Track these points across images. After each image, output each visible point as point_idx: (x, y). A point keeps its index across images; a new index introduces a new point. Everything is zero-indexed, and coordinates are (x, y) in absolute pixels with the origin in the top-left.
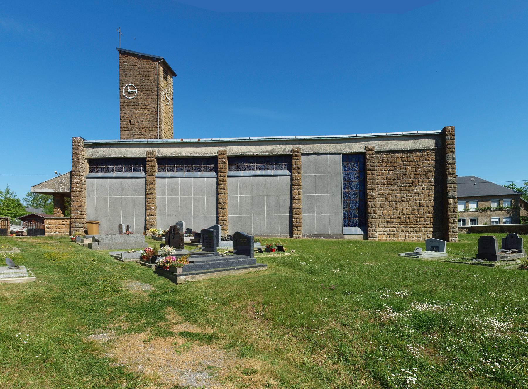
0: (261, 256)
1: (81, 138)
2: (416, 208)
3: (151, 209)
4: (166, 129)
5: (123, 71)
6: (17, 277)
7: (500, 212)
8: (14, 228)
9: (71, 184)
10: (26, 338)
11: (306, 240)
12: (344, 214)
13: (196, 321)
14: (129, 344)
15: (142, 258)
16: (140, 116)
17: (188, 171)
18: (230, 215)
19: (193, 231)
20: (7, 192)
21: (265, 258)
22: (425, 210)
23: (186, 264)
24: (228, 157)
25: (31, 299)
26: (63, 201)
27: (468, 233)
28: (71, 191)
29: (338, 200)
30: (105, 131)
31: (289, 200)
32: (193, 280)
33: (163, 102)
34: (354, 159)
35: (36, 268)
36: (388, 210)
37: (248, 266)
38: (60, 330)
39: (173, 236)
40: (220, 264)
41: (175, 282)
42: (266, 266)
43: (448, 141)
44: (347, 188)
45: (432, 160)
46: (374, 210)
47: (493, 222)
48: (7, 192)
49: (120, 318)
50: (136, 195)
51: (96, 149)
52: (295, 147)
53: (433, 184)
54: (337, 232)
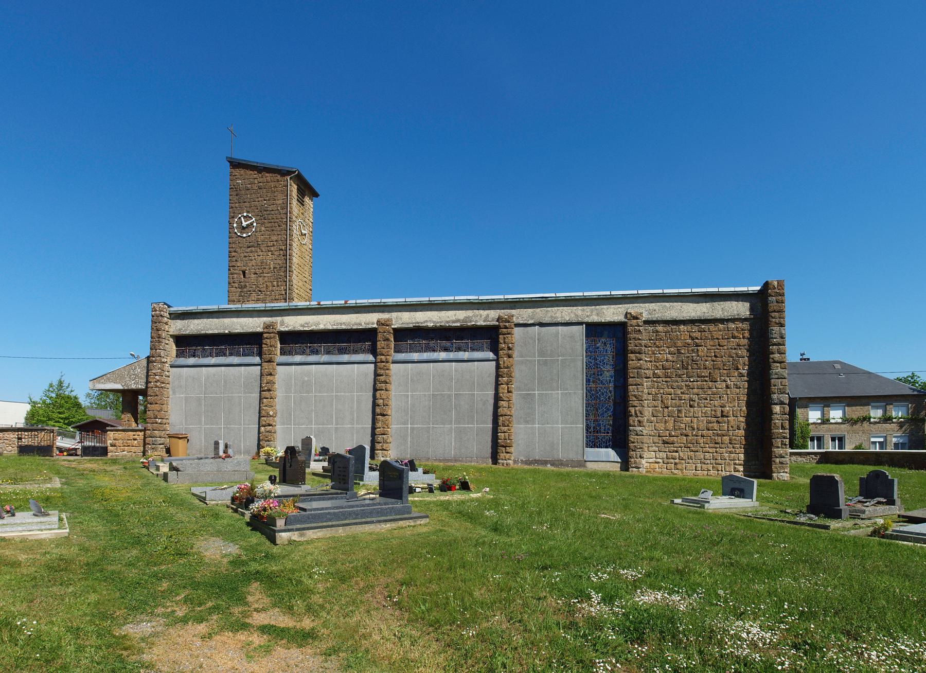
0: (430, 498)
1: (165, 304)
2: (714, 419)
3: (268, 416)
4: (301, 284)
5: (235, 193)
6: (42, 530)
7: (887, 426)
8: (62, 442)
9: (147, 376)
10: (30, 626)
11: (517, 470)
12: (587, 426)
13: (290, 608)
14: (180, 640)
15: (234, 499)
16: (257, 266)
17: (328, 353)
18: (394, 425)
19: (331, 451)
20: (60, 383)
21: (434, 502)
22: (732, 423)
23: (291, 511)
24: (394, 329)
25: (55, 565)
26: (130, 401)
27: (817, 463)
28: (147, 387)
29: (577, 401)
30: (204, 293)
31: (492, 401)
32: (302, 539)
33: (296, 240)
34: (606, 333)
35: (76, 514)
36: (666, 422)
37: (398, 517)
38: (85, 615)
39: (290, 467)
40: (350, 514)
41: (273, 540)
42: (427, 517)
43: (773, 306)
44: (593, 382)
45: (744, 338)
46: (639, 422)
47: (875, 443)
48: (60, 383)
49: (178, 598)
50: (245, 393)
51: (186, 321)
52: (504, 313)
53: (746, 378)
54: (573, 456)
